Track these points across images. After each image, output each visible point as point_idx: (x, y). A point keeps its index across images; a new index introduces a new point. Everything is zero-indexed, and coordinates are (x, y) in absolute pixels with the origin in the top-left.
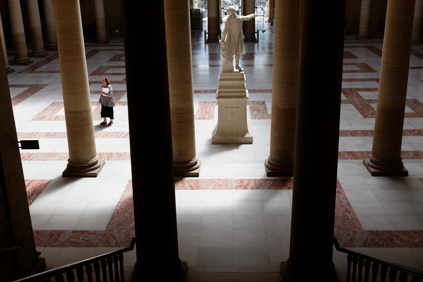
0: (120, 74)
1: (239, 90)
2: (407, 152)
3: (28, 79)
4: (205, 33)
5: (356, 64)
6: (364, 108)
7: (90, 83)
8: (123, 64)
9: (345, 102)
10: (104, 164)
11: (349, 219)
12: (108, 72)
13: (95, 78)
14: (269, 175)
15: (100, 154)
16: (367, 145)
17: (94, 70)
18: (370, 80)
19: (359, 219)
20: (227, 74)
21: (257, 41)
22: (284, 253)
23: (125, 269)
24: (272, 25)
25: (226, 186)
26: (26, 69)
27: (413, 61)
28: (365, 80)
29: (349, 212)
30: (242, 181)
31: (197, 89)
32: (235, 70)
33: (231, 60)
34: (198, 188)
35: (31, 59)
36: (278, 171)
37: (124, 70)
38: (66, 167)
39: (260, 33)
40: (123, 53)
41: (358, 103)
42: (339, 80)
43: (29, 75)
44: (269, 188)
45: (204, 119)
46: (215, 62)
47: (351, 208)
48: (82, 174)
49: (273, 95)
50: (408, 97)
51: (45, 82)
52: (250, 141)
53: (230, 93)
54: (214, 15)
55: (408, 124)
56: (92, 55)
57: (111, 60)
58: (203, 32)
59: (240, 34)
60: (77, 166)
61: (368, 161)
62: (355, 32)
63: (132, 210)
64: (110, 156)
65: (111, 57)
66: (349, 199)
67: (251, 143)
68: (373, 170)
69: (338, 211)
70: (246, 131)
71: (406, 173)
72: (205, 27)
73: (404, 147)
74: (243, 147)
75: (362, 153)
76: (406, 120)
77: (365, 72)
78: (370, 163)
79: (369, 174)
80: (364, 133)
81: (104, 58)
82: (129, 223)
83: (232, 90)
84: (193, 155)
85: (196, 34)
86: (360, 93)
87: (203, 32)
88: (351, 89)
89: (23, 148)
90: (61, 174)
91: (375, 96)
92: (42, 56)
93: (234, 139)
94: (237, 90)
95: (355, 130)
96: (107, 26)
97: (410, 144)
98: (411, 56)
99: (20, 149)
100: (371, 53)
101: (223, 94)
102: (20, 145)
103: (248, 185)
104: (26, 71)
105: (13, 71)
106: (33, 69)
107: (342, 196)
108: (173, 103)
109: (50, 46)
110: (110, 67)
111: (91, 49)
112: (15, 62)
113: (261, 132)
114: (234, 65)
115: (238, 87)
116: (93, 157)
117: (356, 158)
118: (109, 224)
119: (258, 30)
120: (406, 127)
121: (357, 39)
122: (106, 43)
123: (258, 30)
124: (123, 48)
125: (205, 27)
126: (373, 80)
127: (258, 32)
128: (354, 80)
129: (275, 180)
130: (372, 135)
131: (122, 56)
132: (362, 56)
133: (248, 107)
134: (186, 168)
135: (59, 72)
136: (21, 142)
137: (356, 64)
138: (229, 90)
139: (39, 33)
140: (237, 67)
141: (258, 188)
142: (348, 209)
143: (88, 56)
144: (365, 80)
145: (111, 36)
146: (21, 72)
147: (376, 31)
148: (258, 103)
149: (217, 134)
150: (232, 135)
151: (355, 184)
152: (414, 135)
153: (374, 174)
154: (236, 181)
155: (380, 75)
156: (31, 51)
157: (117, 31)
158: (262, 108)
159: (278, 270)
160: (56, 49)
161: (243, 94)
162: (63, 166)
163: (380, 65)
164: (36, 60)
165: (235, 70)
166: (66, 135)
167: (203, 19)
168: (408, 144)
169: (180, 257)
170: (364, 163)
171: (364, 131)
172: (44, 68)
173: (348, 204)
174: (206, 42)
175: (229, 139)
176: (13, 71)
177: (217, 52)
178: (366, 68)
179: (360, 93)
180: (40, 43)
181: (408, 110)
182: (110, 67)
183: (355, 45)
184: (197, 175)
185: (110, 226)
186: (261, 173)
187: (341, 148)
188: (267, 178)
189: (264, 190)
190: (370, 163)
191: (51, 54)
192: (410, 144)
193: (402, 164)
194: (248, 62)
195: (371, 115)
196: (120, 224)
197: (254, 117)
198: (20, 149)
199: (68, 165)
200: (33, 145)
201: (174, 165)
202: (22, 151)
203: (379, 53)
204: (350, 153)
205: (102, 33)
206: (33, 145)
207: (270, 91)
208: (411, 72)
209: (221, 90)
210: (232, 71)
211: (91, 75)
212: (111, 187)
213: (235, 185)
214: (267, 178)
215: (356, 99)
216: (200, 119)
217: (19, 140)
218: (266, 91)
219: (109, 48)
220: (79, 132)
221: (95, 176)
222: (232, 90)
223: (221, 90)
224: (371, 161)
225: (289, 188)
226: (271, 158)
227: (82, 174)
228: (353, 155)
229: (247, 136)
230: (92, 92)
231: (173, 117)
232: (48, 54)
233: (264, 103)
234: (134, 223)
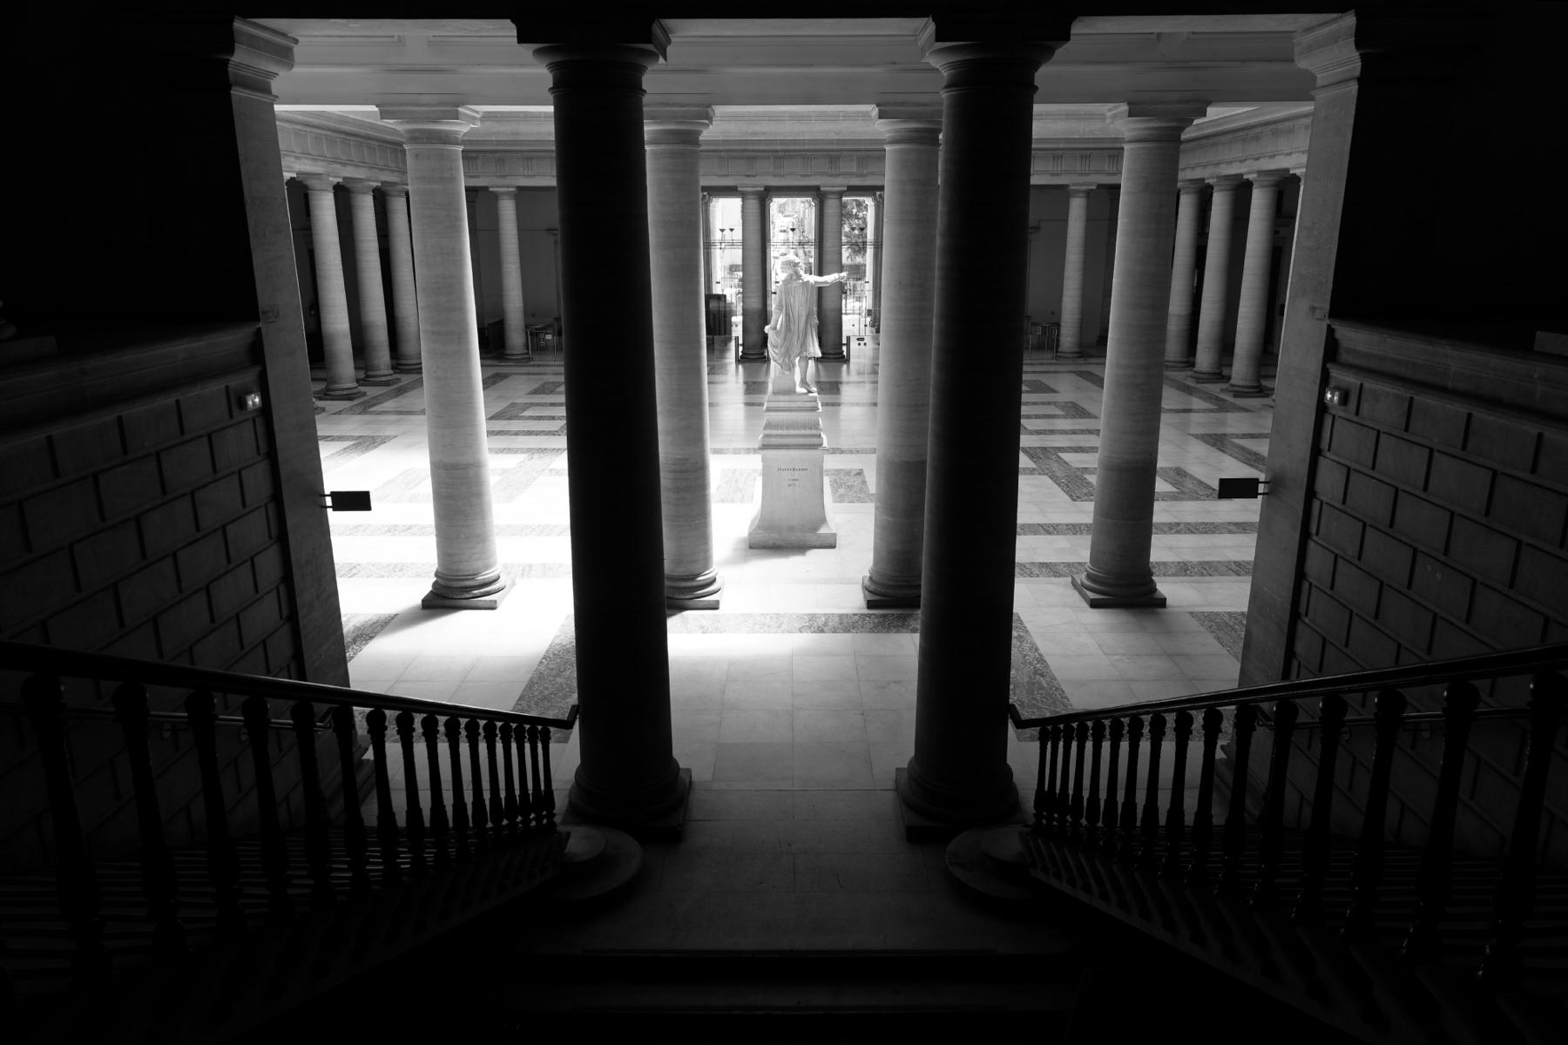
0: (553, 418)
1: (808, 432)
2: (1164, 564)
3: (353, 425)
4: (737, 345)
5: (1055, 404)
6: (1072, 484)
7: (490, 433)
8: (562, 399)
9: (1032, 472)
10: (514, 584)
11: (1042, 688)
12: (526, 414)
13: (500, 425)
14: (871, 605)
15: (505, 566)
16: (1080, 551)
17: (499, 407)
18: (1083, 432)
19: (1064, 687)
20: (781, 398)
21: (846, 360)
22: (902, 748)
23: (554, 786)
24: (878, 331)
25: (778, 615)
26: (351, 409)
27: (1170, 398)
28: (1074, 432)
29: (1042, 675)
30: (813, 617)
31: (717, 446)
32: (800, 390)
33: (791, 367)
34: (717, 630)
35: (363, 389)
36: (889, 598)
37: (562, 411)
38: (430, 588)
39: (854, 344)
40: (562, 379)
41: (1059, 473)
42: (1018, 404)
43: (357, 418)
44: (871, 631)
45: (733, 501)
46: (756, 398)
47: (1047, 667)
48: (465, 602)
49: (879, 461)
50: (1161, 463)
51: (389, 431)
52: (831, 541)
53: (787, 440)
54: (755, 303)
55: (1161, 513)
56: (494, 383)
57: (535, 392)
58: (733, 344)
59: (809, 316)
60: (455, 584)
61: (1082, 578)
62: (1049, 344)
63: (572, 673)
64: (527, 570)
65: (535, 386)
66: (1042, 651)
67: (833, 546)
68: (1091, 595)
69: (1018, 673)
70: (823, 520)
71: (1162, 603)
72: (737, 331)
73: (1156, 555)
74: (813, 554)
75: (1068, 565)
76: (1158, 506)
77: (1074, 417)
78: (1087, 583)
79: (1085, 605)
80: (1074, 529)
81: (519, 387)
82: (565, 697)
83: (792, 432)
84: (706, 563)
85: (717, 346)
86: (1062, 455)
87: (733, 344)
88: (1044, 449)
89: (336, 507)
90: (419, 602)
91: (1092, 461)
92: (386, 384)
93: (794, 537)
94: (803, 432)
95: (1052, 523)
96: (527, 326)
97: (1170, 548)
98: (1164, 394)
99: (330, 511)
100: (1085, 383)
101: (773, 441)
102: (329, 501)
103: (826, 624)
104: (351, 411)
105: (323, 410)
106: (365, 408)
107: (1026, 646)
108: (666, 449)
109: (404, 365)
110: (532, 404)
111: (493, 371)
112: (326, 395)
113: (856, 538)
114: (797, 378)
115: (804, 426)
116: (487, 567)
117: (1057, 574)
118: (521, 698)
119: (848, 338)
120: (1158, 517)
121: (1057, 358)
122: (525, 360)
123: (848, 338)
124: (562, 370)
125: (737, 331)
126: (1090, 432)
127: (848, 345)
128: (1052, 432)
129: (885, 616)
130: (1088, 532)
131: (559, 384)
132: (1067, 387)
133: (826, 480)
134: (690, 592)
135: (423, 412)
136: (333, 495)
137: (1055, 404)
138: (785, 432)
139: (380, 335)
140: (804, 383)
141: (847, 630)
142: (1040, 667)
143: (487, 383)
144: (1074, 432)
145: (535, 345)
146: (339, 413)
147: (1093, 345)
148: (848, 473)
149: (759, 527)
150: (791, 529)
151: (1059, 632)
152: (1178, 532)
153: (1094, 604)
154: (800, 617)
155: (1101, 424)
156: (362, 375)
157: (549, 337)
158: (857, 481)
159: (891, 785)
160: (419, 371)
161: (815, 441)
162: (425, 587)
163: (1104, 402)
164: (372, 391)
165: (800, 390)
166: (433, 530)
167: (734, 319)
168: (1161, 550)
169: (677, 752)
170: (1074, 583)
171: (1074, 526)
172: (389, 405)
173: (1041, 660)
174: (739, 361)
175: (781, 538)
176: (323, 410)
177: (762, 379)
178: (1077, 411)
179: (1062, 455)
180: (383, 356)
181: (1161, 486)
182: (532, 404)
183: (1052, 368)
184: (714, 606)
185: (524, 703)
186: (853, 601)
187: (1020, 557)
188: (866, 611)
189: (859, 635)
190: (1087, 583)
191: (406, 379)
192: (1170, 548)
193: (1152, 583)
194: (829, 398)
195: (1087, 496)
196: (545, 698)
197: (840, 499)
198: (330, 511)
199: (435, 584)
200: (357, 501)
201: (667, 583)
202: (336, 519)
203: (1099, 382)
204: (1043, 565)
205: (516, 338)
206: (357, 501)
207: (874, 451)
208: (1164, 417)
209: (768, 432)
210: (792, 391)
211: (490, 418)
212: (530, 619)
213: (798, 626)
214: (866, 611)
215: (1055, 467)
216: (722, 501)
217: (327, 492)
218: (865, 451)
219: (531, 370)
220: (458, 500)
221: (492, 607)
222: (792, 432)
223: (768, 432)
224: (1089, 576)
225: (914, 631)
226: (873, 572)
227: (465, 602)
228: (1051, 569)
229: (823, 531)
230: (491, 450)
231: (665, 479)
232: (399, 380)
233: (860, 473)
234: (576, 696)
